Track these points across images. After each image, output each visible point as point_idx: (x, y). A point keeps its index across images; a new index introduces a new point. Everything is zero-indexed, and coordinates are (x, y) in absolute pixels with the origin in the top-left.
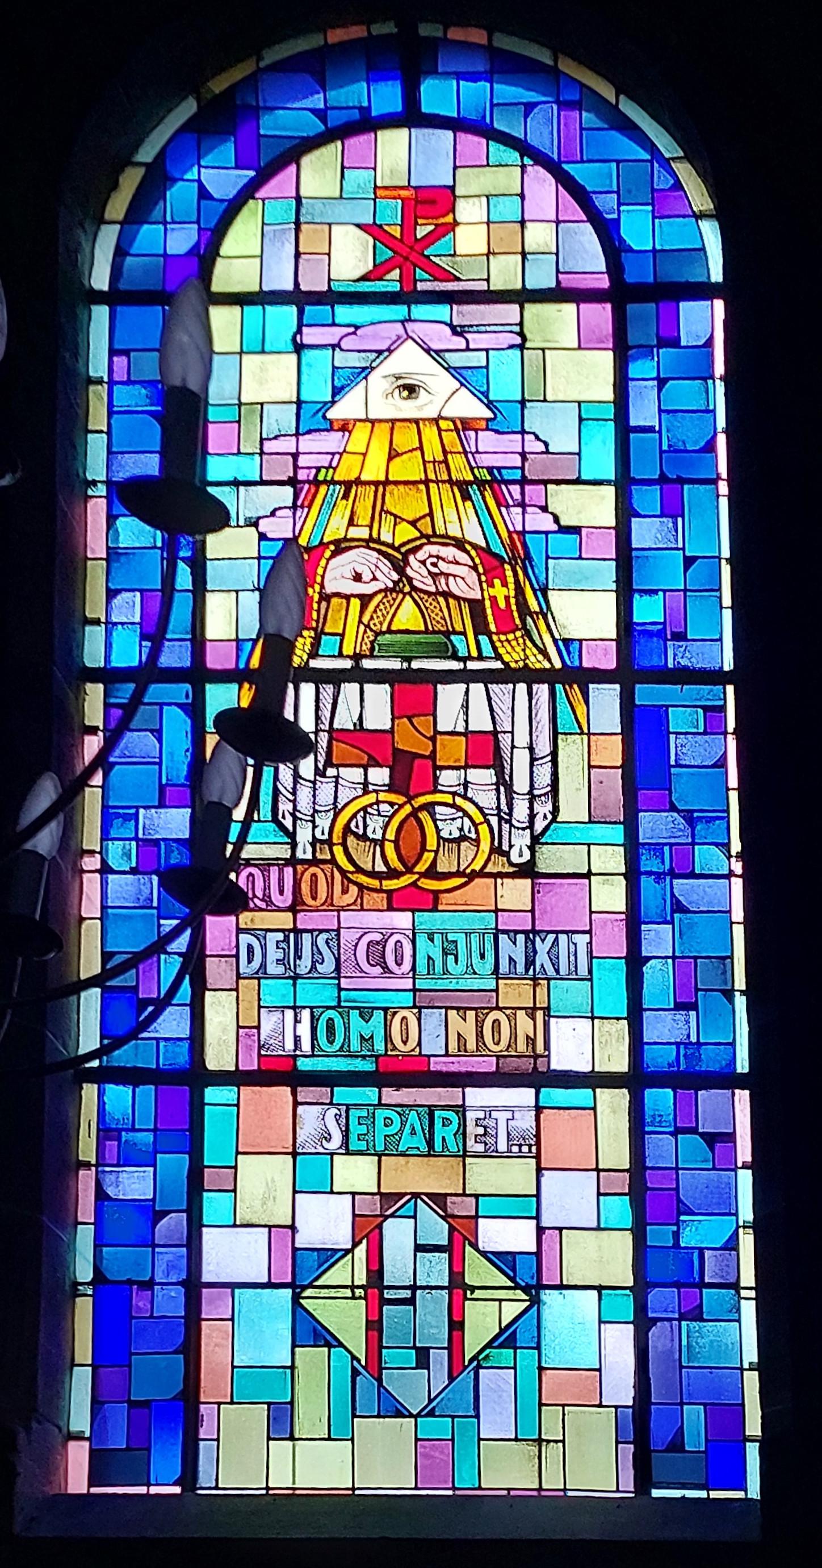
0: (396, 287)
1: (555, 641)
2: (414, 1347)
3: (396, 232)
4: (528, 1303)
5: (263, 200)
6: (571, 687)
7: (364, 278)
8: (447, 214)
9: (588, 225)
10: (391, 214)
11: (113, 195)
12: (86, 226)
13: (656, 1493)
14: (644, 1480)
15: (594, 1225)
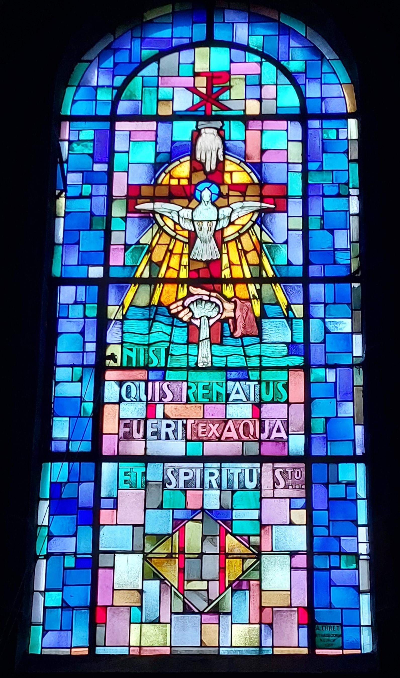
0: (203, 113)
1: (271, 266)
2: (82, 185)
3: (204, 91)
4: (255, 560)
5: (143, 77)
6: (275, 285)
7: (188, 110)
8: (227, 82)
9: (292, 86)
10: (201, 82)
11: (72, 75)
12: (152, 94)
13: (318, 652)
14: (312, 645)
15: (272, 496)
